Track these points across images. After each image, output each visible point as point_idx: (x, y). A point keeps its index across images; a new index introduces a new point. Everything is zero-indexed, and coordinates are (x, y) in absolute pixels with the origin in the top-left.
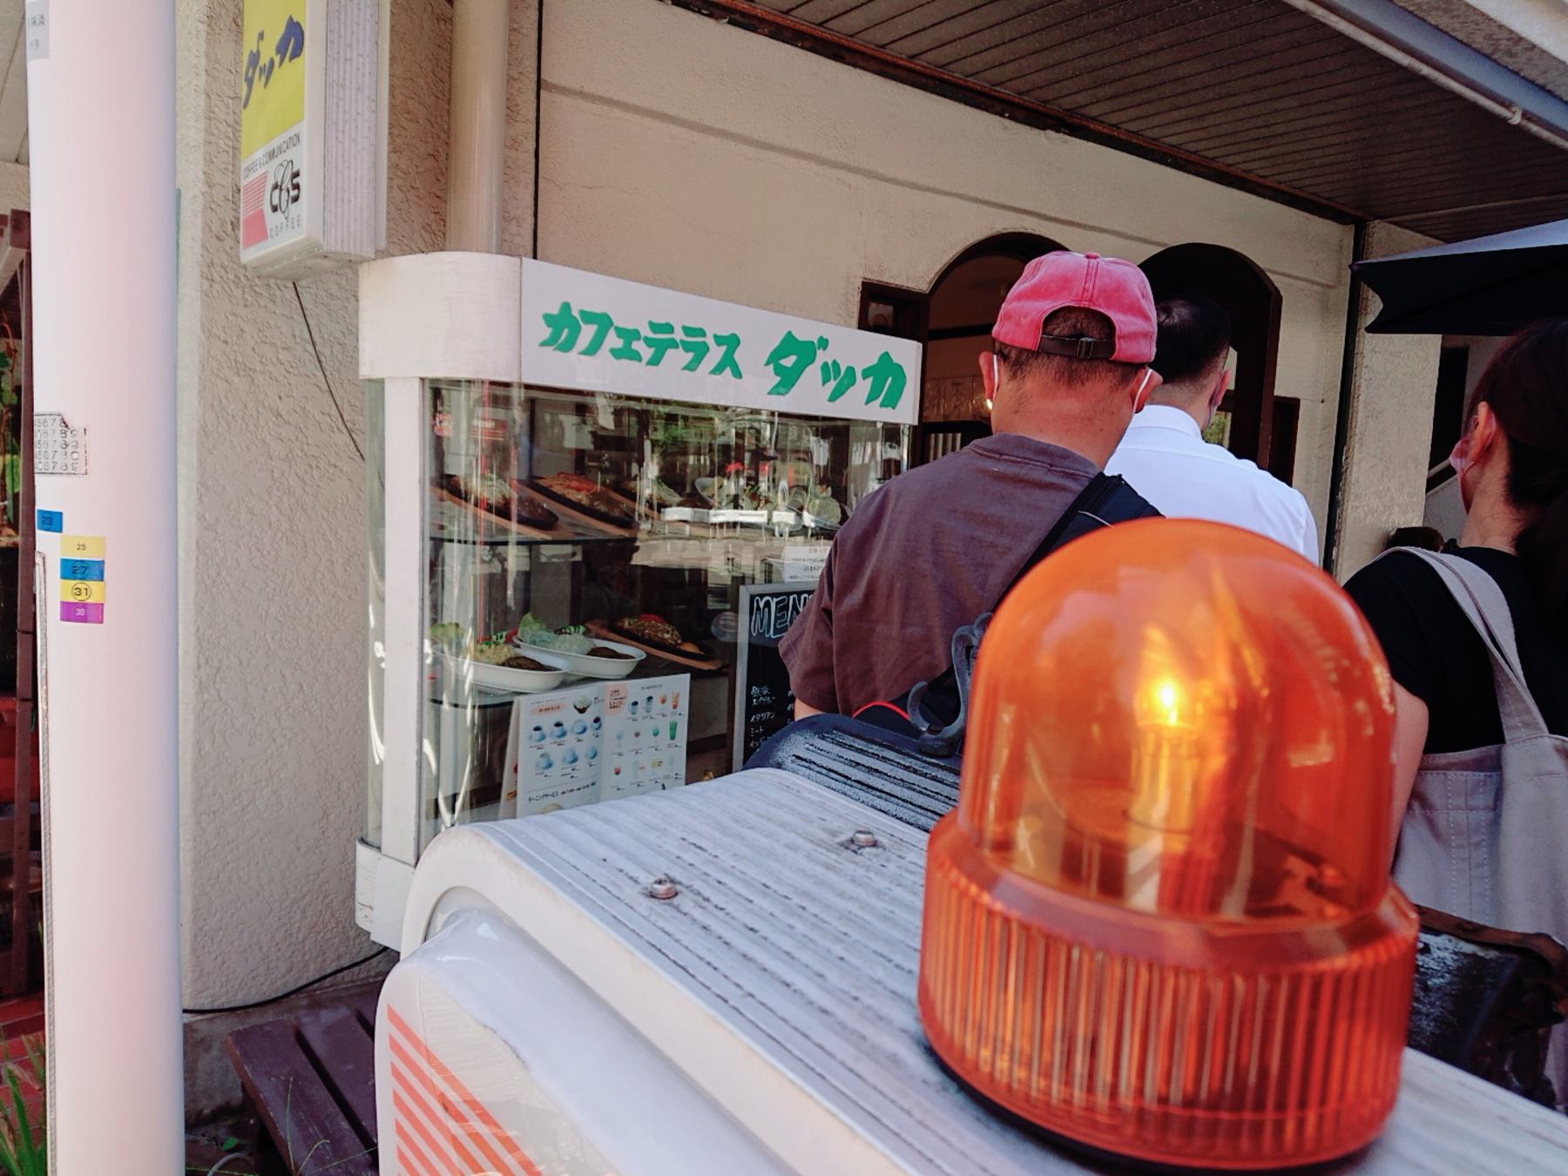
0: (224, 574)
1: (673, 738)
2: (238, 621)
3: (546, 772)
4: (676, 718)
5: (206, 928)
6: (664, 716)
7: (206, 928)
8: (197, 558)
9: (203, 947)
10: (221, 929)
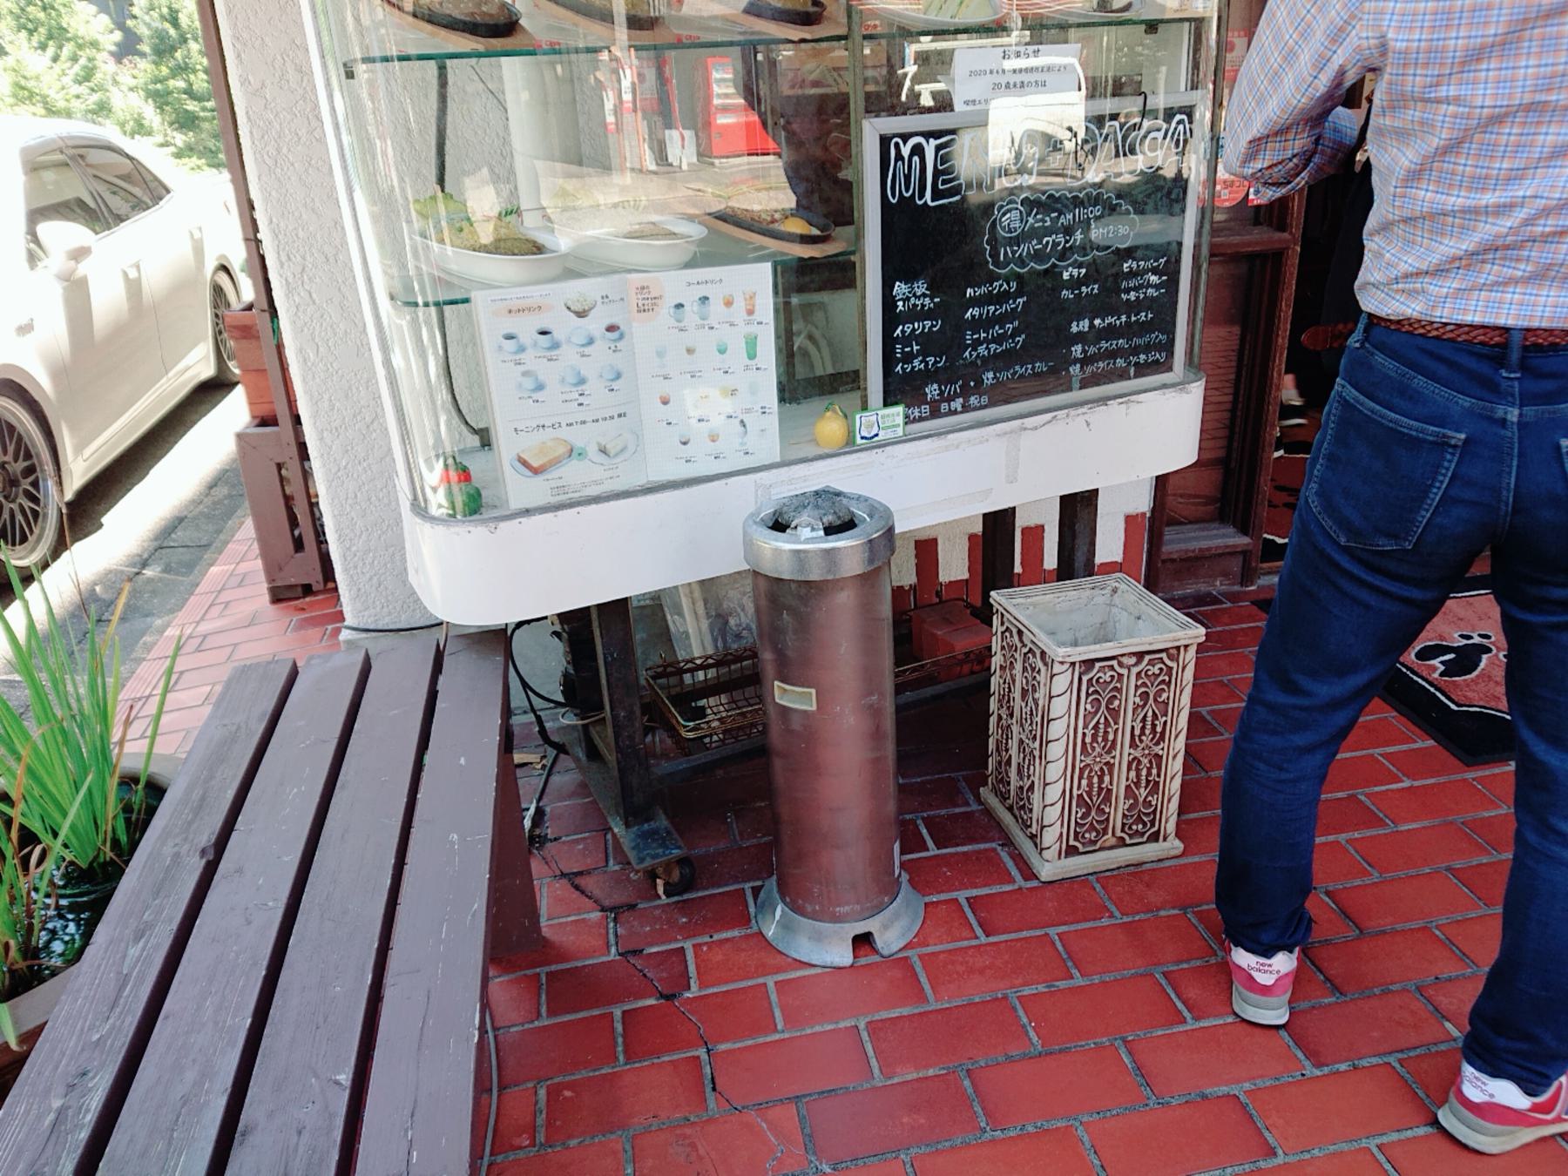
0: (285, 150)
1: (752, 356)
2: (313, 210)
3: (536, 396)
4: (754, 329)
5: (354, 549)
6: (732, 325)
7: (354, 549)
8: (251, 133)
9: (356, 567)
10: (370, 550)
